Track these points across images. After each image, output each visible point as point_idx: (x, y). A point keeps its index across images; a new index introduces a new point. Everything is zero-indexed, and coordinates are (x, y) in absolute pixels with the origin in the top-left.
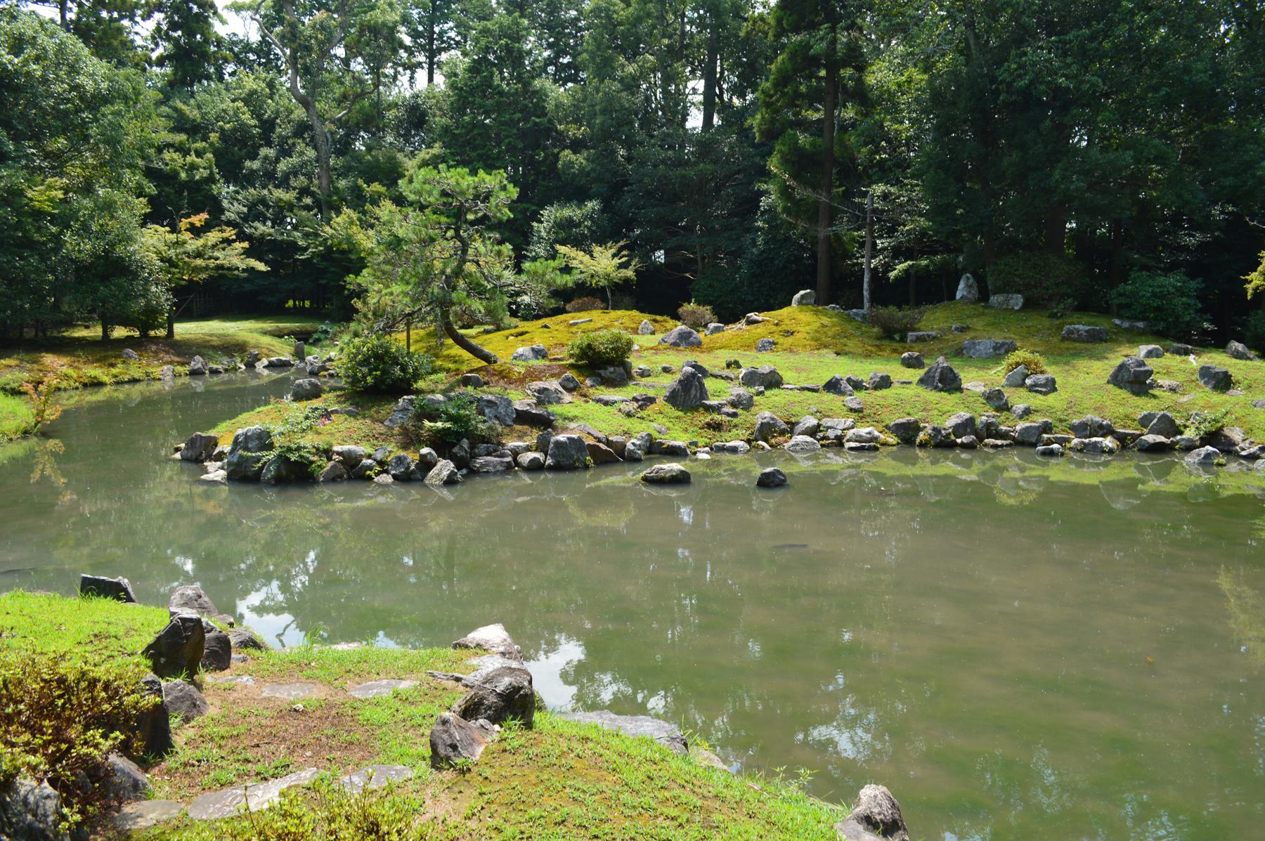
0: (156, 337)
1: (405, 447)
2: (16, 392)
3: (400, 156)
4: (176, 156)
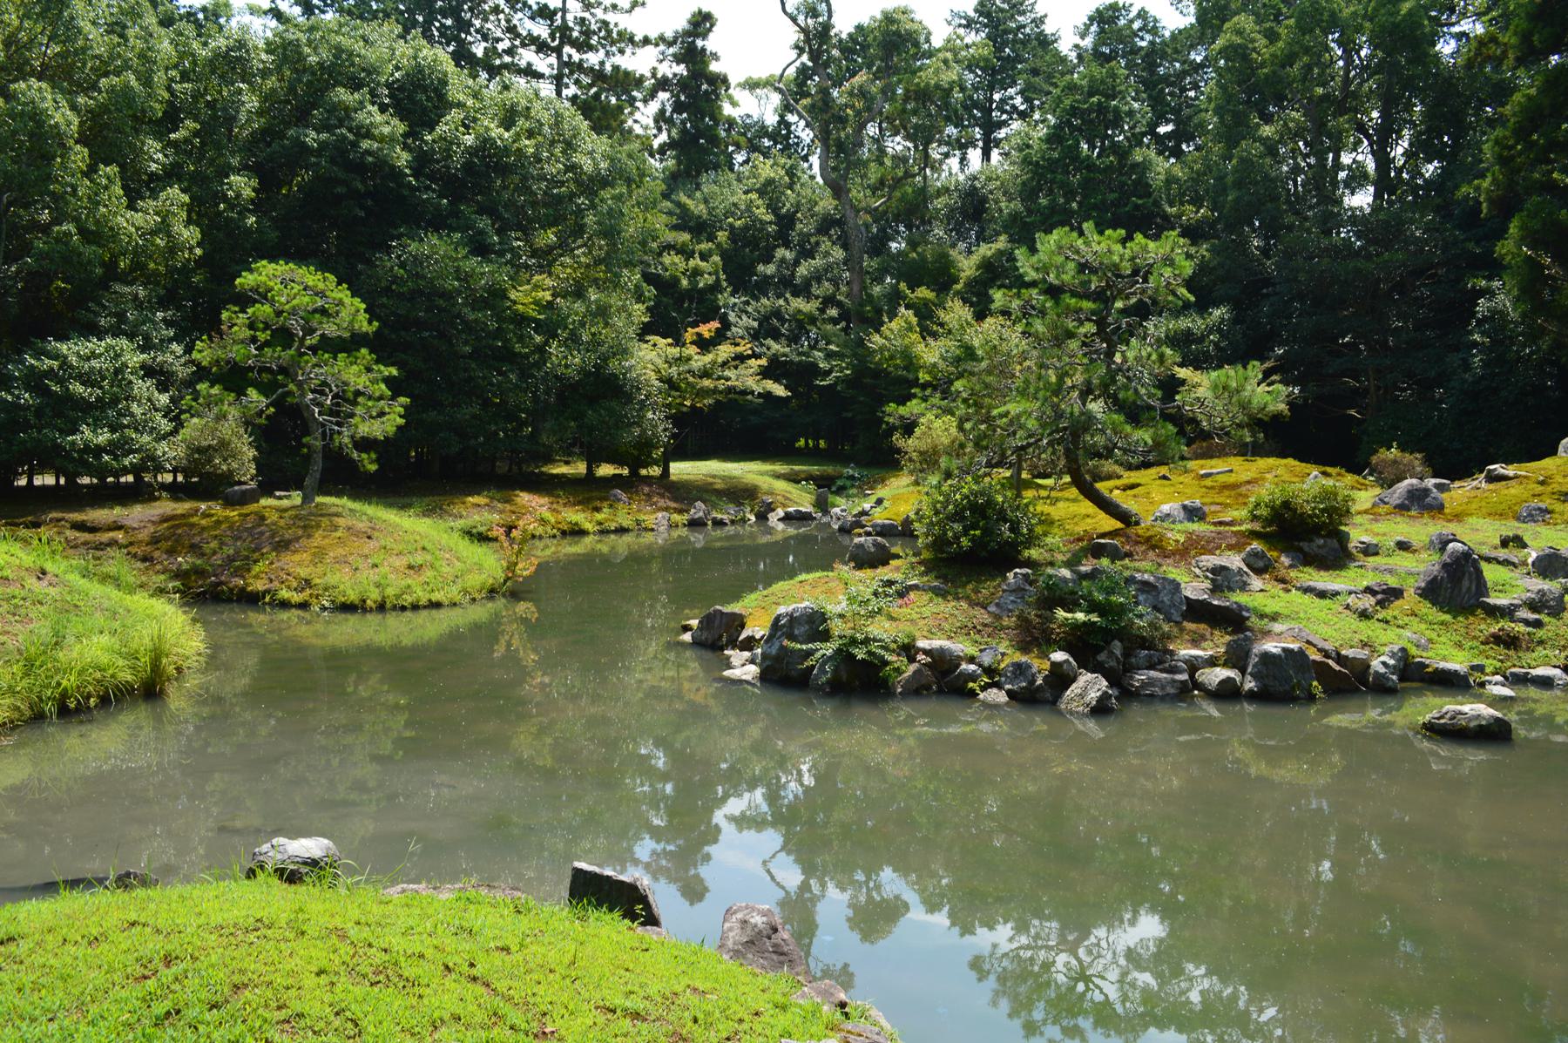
0: (648, 477)
1: (1024, 648)
2: (483, 538)
3: (953, 253)
4: (677, 259)
